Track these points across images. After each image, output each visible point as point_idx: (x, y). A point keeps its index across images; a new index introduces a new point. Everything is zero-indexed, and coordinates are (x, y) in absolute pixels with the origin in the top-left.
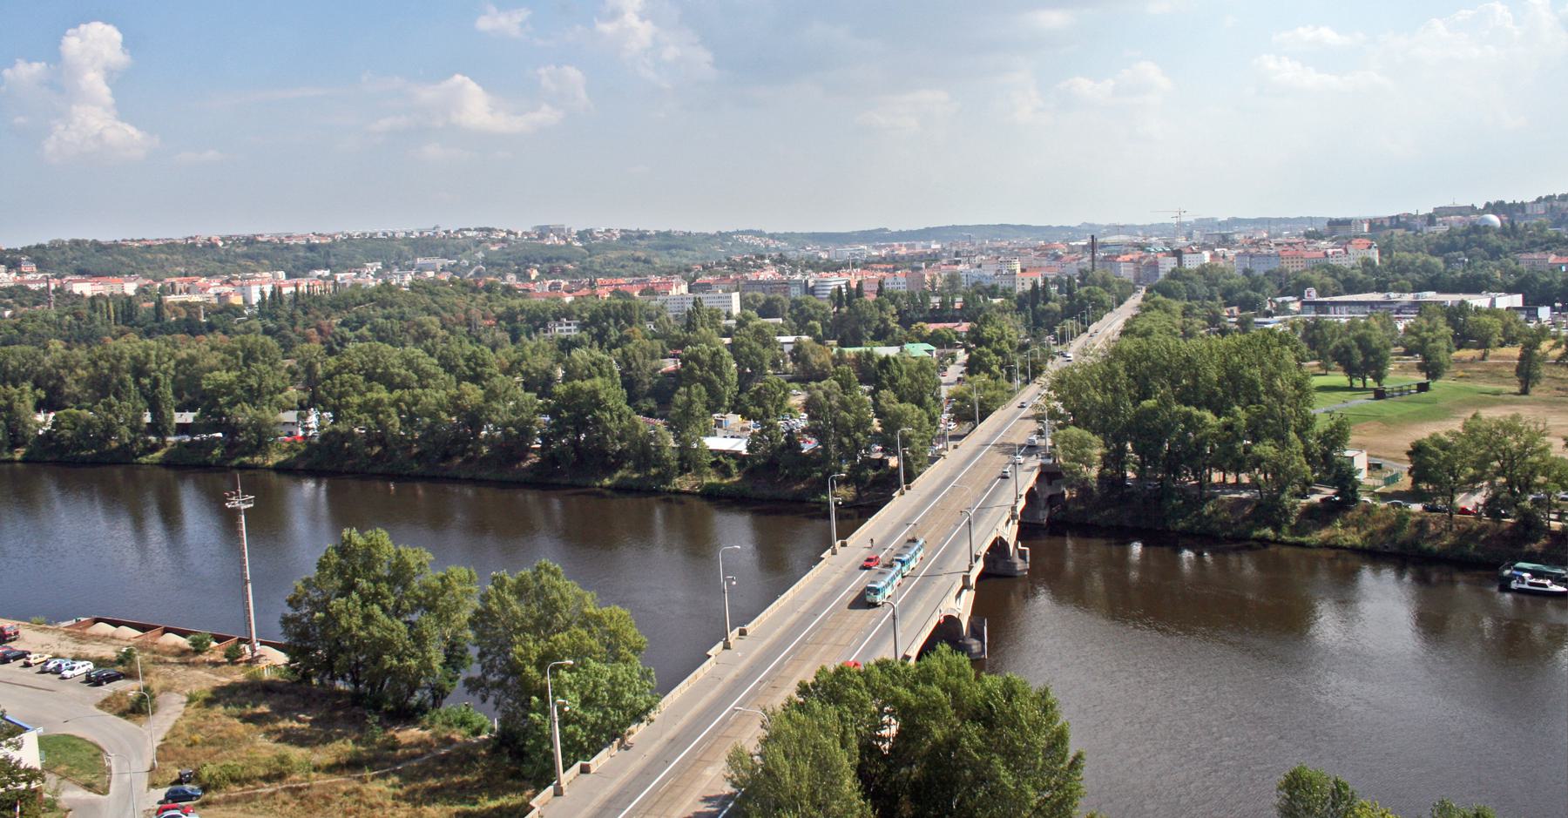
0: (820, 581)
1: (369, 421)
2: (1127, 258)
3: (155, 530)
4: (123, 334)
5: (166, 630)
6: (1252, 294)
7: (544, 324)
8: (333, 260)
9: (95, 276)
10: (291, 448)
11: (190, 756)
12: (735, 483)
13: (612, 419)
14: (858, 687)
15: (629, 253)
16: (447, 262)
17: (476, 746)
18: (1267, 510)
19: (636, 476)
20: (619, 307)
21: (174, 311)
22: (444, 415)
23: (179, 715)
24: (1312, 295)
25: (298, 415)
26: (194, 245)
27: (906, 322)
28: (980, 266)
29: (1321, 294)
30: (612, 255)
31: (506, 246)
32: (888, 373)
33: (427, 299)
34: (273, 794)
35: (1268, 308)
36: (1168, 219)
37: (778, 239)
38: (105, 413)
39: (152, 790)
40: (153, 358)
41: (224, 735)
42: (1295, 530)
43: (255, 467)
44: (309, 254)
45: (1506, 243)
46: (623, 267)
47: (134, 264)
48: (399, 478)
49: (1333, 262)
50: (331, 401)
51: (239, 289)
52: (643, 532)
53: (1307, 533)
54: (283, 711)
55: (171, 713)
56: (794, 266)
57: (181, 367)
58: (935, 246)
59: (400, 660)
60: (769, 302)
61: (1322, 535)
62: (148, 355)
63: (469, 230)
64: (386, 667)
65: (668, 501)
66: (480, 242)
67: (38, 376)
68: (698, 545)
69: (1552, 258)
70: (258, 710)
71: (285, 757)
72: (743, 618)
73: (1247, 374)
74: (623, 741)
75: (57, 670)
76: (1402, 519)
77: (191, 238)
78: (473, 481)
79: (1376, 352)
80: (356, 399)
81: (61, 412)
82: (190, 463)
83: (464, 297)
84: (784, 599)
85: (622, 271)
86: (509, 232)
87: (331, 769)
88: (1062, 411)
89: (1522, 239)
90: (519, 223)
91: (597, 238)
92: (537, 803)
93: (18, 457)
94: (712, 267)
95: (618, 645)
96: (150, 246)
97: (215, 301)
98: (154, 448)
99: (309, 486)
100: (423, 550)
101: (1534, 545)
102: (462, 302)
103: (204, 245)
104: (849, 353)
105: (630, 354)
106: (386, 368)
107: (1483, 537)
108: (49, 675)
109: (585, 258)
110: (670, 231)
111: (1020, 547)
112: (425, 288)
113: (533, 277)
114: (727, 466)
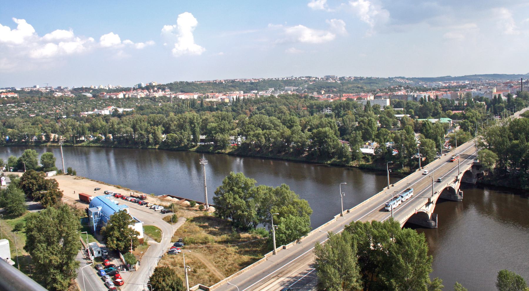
1: (256, 140)
3: (194, 171)
4: (191, 111)
5: (186, 200)
7: (322, 110)
8: (258, 88)
9: (187, 92)
10: (233, 148)
11: (183, 235)
12: (370, 164)
13: (331, 141)
14: (361, 228)
15: (356, 85)
16: (295, 88)
17: (263, 240)
19: (338, 160)
20: (345, 104)
21: (207, 104)
22: (279, 139)
23: (183, 224)
25: (235, 137)
26: (216, 83)
27: (444, 109)
28: (480, 90)
30: (350, 86)
31: (315, 82)
33: (285, 100)
34: (202, 247)
37: (410, 80)
38: (180, 135)
39: (171, 243)
40: (195, 118)
41: (193, 230)
43: (222, 153)
44: (251, 86)
46: (353, 90)
47: (198, 89)
48: (265, 158)
50: (245, 133)
51: (228, 97)
52: (340, 180)
54: (211, 225)
55: (181, 223)
56: (412, 90)
57: (204, 122)
58: (467, 82)
59: (243, 212)
62: (194, 118)
63: (303, 77)
64: (239, 214)
65: (348, 169)
66: (307, 81)
67: (164, 124)
68: (358, 184)
70: (205, 224)
71: (207, 237)
72: (348, 207)
74: (298, 241)
75: (154, 208)
77: (215, 80)
78: (288, 160)
80: (252, 133)
81: (168, 134)
82: (203, 151)
83: (297, 100)
84: (366, 202)
85: (353, 91)
86: (316, 78)
87: (220, 243)
90: (319, 74)
91: (346, 80)
92: (266, 256)
93: (157, 147)
94: (383, 90)
95: (303, 212)
96: (203, 83)
97: (220, 101)
98: (194, 146)
99: (238, 160)
100: (254, 179)
102: (296, 101)
103: (219, 83)
105: (345, 120)
106: (264, 123)
108: (152, 209)
109: (341, 87)
110: (371, 77)
111: (460, 191)
112: (284, 97)
113: (322, 93)
114: (368, 159)
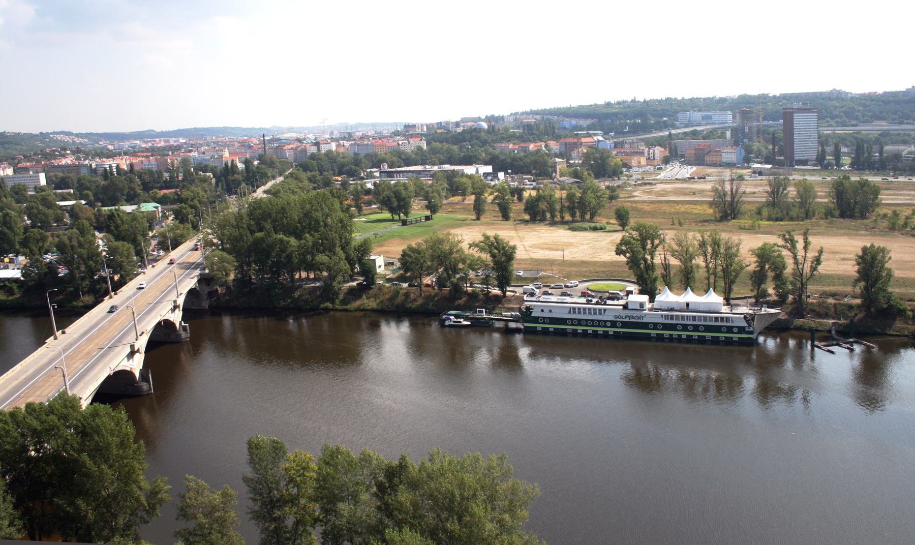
0: (42, 356)
2: (290, 147)
6: (353, 167)
18: (328, 292)
24: (385, 167)
29: (390, 167)
37: (81, 137)
42: (344, 302)
45: (489, 138)
49: (402, 148)
53: (350, 303)
58: (182, 141)
60: (63, 179)
61: (357, 304)
69: (511, 146)
73: (314, 215)
76: (397, 293)
79: (404, 199)
88: (215, 241)
89: (497, 135)
101: (460, 301)
104: (105, 211)
107: (436, 298)
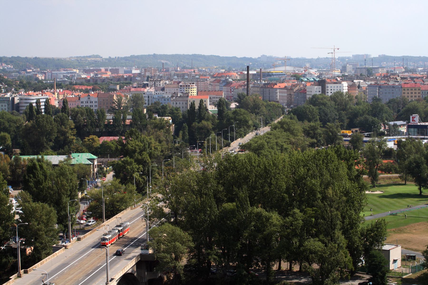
2: (283, 85)
24: (416, 119)
28: (163, 89)
32: (34, 177)
35: (382, 129)
36: (323, 54)
104: (24, 160)
